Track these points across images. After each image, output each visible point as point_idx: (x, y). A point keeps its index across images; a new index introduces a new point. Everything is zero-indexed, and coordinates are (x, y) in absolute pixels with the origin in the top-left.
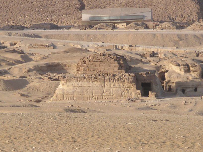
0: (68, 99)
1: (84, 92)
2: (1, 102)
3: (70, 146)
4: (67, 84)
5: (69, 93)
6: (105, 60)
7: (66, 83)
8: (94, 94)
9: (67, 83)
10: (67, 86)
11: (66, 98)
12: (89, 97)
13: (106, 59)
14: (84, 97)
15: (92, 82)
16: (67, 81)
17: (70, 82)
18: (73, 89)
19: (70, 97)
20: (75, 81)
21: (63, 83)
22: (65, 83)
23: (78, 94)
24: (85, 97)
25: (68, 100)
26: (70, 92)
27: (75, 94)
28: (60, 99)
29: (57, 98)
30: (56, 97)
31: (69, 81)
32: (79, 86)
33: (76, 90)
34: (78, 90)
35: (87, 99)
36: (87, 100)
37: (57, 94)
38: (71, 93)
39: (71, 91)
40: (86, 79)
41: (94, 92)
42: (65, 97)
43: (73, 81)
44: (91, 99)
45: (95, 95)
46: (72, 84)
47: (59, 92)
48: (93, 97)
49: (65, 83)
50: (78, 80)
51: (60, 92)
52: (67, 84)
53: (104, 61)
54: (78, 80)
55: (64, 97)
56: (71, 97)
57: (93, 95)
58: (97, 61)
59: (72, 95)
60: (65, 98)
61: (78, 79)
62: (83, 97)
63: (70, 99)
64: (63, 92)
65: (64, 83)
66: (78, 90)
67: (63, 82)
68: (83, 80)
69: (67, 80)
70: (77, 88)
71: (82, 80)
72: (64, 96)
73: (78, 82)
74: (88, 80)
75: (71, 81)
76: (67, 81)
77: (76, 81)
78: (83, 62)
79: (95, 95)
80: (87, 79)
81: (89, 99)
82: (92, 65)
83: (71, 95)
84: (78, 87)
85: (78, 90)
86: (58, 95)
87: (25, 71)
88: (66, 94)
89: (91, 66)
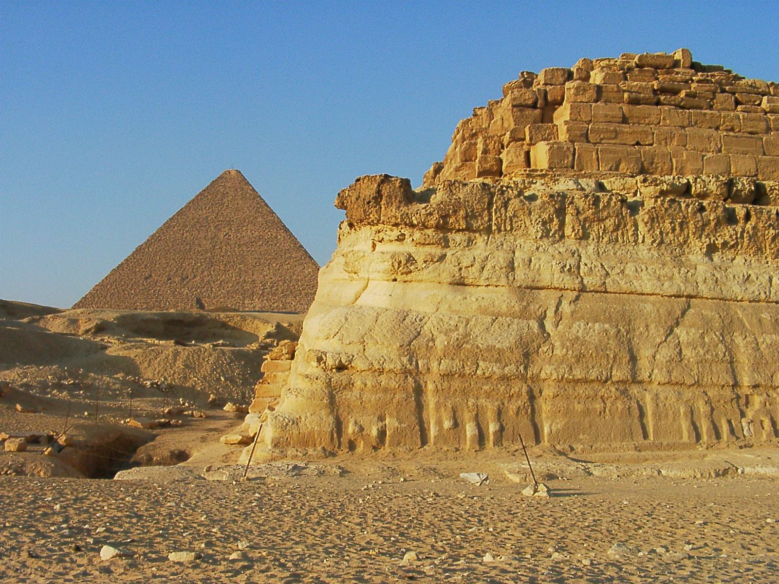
0: (470, 430)
1: (645, 354)
2: (777, 303)
3: (197, 502)
4: (442, 258)
5: (476, 356)
6: (720, 97)
7: (437, 251)
8: (746, 381)
9: (446, 244)
10: (446, 278)
11: (447, 424)
12: (702, 408)
13: (723, 91)
14: (649, 410)
15: (711, 249)
16: (443, 227)
17: (480, 240)
18: (524, 314)
19: (490, 408)
20: (535, 230)
21: (396, 247)
22: (420, 254)
23: (578, 373)
24: (657, 416)
25: (481, 438)
26: (490, 349)
27: (547, 370)
28: (382, 434)
29: (339, 425)
30: (332, 397)
31: (469, 229)
32: (583, 289)
33: (549, 326)
34: (571, 331)
35: (685, 425)
36: (685, 446)
37: (341, 368)
38: (499, 356)
39: (504, 338)
40: (642, 216)
41: (744, 358)
42: (430, 400)
43: (509, 226)
44: (725, 429)
45: (756, 386)
46: (501, 258)
47: (354, 349)
48: (743, 415)
49: (420, 254)
50: (562, 224)
51: (372, 351)
52: (442, 258)
53: (711, 107)
54: (568, 218)
55: (420, 407)
56: (512, 407)
57: (736, 385)
58: (658, 103)
59: (519, 387)
60: (437, 421)
61: (561, 212)
62: (642, 415)
63: (492, 428)
64: (409, 350)
65: (408, 247)
66: (578, 328)
67: (401, 239)
68: (617, 228)
69: (445, 217)
70: (566, 308)
71: (610, 223)
72: (419, 391)
73: (571, 243)
74: (667, 225)
75: (488, 231)
76: (443, 227)
77: (546, 234)
78: (534, 106)
79: (756, 386)
80: (653, 220)
81: (704, 426)
82: (626, 128)
83: (504, 378)
84: (572, 295)
85: (578, 328)
86: (350, 385)
87: (88, 327)
88: (448, 376)
89: (616, 133)
